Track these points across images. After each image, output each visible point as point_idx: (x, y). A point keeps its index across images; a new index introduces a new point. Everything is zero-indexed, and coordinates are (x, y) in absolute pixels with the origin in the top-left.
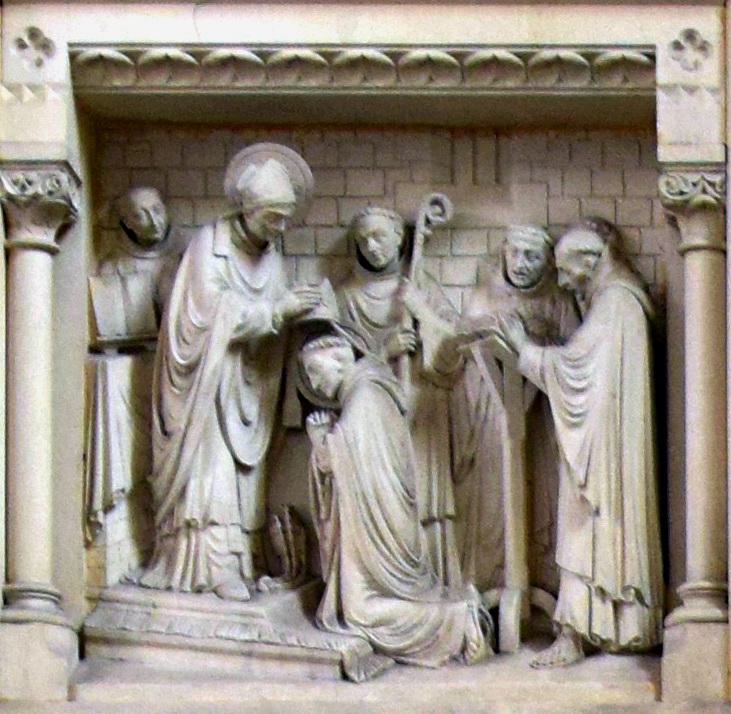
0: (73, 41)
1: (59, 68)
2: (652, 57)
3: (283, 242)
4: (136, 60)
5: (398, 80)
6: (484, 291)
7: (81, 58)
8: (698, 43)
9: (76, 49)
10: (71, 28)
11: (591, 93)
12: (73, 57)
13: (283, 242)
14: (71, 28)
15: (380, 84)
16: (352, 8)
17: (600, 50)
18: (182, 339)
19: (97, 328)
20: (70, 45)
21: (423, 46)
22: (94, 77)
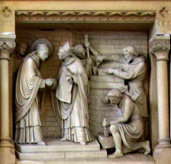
0: (16, 10)
1: (12, 19)
2: (155, 14)
3: (113, 82)
4: (30, 14)
5: (30, 19)
6: (121, 97)
7: (18, 14)
8: (8, 10)
9: (17, 12)
10: (14, 6)
11: (99, 22)
12: (16, 13)
13: (113, 82)
14: (14, 6)
15: (41, 20)
16: (59, 2)
17: (95, 12)
18: (36, 141)
19: (129, 152)
20: (16, 11)
21: (100, 11)
22: (20, 19)
